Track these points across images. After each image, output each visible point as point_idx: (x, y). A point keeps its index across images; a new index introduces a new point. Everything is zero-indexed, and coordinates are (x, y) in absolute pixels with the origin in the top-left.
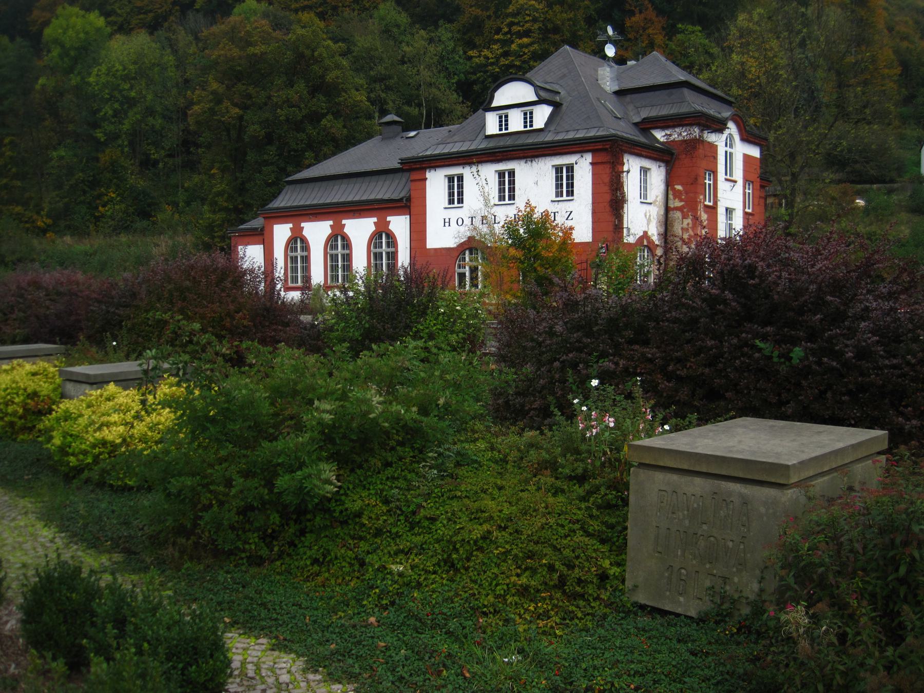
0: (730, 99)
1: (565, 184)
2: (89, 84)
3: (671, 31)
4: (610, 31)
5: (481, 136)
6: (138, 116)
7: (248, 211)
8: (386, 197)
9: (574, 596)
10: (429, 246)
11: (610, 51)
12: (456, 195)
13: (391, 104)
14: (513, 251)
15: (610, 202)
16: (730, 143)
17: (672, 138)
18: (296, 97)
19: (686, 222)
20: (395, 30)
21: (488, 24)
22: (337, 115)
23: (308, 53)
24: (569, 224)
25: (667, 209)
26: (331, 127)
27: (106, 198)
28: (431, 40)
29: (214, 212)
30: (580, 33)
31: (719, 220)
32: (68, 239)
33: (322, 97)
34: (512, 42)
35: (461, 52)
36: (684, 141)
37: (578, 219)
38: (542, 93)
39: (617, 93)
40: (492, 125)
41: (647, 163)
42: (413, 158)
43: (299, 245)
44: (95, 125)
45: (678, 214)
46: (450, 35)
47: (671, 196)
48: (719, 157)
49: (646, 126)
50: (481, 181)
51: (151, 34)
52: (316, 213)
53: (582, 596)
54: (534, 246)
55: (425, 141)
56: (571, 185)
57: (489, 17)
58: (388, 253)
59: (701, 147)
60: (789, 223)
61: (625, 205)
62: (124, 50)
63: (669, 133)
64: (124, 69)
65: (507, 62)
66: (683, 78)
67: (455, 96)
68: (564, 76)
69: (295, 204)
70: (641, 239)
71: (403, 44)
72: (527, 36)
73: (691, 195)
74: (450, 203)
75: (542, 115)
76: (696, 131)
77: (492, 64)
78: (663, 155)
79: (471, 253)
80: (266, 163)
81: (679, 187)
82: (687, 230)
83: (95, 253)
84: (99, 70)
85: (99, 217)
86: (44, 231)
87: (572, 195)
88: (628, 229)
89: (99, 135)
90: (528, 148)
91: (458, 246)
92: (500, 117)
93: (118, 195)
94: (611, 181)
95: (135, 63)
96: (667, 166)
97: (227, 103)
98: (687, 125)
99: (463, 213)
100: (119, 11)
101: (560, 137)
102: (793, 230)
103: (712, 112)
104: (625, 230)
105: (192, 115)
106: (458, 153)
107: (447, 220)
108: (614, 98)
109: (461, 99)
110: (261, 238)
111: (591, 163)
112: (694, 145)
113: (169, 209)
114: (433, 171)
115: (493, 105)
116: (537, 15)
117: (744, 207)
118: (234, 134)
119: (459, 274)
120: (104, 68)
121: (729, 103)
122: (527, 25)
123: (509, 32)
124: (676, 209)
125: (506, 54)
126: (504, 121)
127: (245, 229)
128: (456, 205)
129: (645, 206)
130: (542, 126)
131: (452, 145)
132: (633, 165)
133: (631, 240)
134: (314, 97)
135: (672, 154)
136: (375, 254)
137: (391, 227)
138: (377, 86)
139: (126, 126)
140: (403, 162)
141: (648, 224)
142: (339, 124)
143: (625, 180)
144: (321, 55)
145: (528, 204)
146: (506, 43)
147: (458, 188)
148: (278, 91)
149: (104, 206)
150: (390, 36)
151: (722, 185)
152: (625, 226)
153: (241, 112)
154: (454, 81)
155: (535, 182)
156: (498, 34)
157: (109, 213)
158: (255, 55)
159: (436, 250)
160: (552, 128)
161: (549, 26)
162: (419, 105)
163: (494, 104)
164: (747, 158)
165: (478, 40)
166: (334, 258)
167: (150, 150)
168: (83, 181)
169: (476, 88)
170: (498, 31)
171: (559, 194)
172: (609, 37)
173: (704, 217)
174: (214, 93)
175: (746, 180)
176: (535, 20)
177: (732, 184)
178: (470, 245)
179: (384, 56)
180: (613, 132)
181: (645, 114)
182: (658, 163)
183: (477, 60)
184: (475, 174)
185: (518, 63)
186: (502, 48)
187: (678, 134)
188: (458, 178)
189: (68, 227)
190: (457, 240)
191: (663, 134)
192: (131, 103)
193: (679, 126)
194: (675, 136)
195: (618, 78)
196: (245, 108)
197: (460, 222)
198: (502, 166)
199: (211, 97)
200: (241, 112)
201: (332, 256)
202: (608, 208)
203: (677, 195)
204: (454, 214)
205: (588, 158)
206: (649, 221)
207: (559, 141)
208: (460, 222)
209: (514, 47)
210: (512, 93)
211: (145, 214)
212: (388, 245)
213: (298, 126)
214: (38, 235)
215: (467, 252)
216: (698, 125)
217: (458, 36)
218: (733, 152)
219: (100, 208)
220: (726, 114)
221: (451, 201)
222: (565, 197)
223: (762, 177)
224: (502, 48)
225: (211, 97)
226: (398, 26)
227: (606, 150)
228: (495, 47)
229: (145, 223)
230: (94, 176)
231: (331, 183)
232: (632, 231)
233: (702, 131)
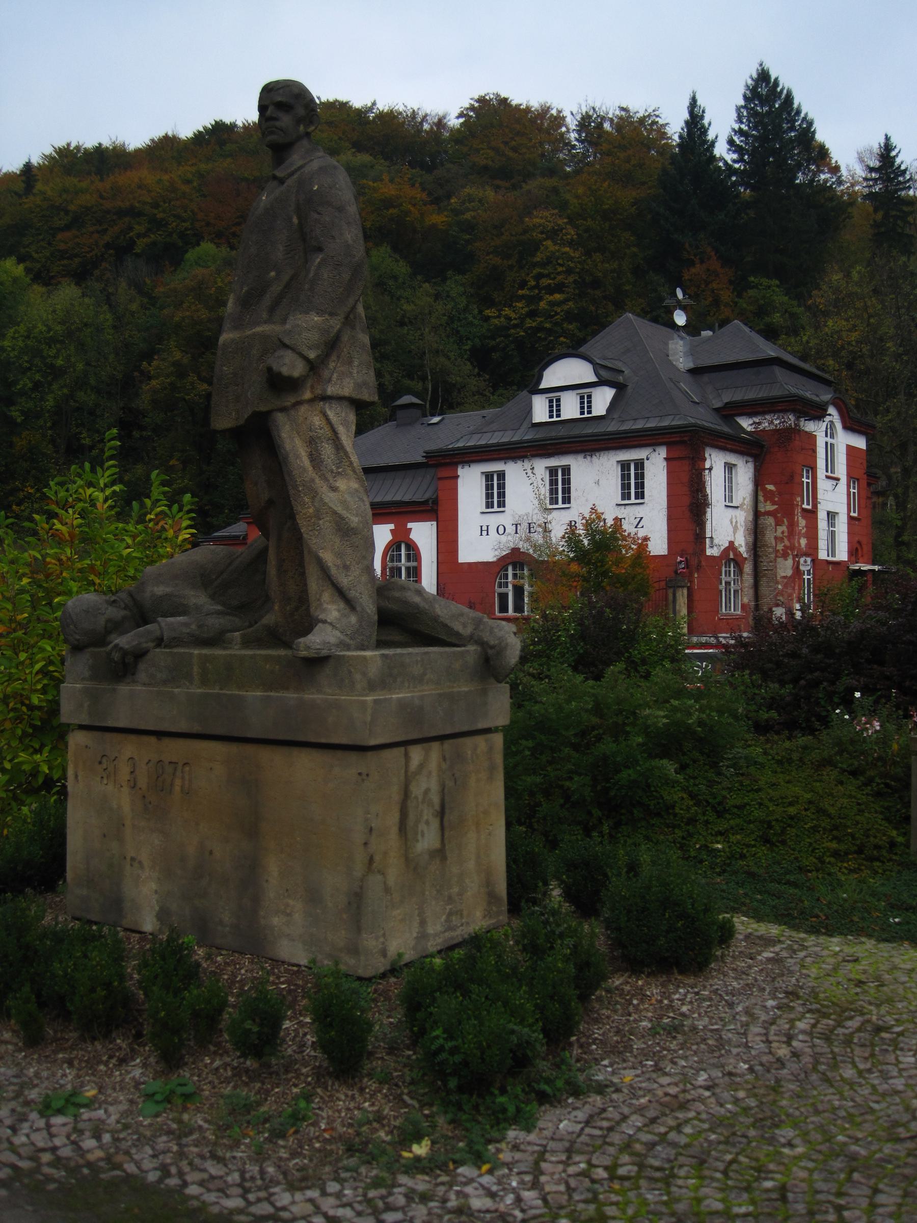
0: (826, 376)
1: (633, 485)
3: (740, 286)
4: (680, 294)
5: (526, 425)
6: (65, 391)
8: (407, 498)
9: (872, 859)
10: (461, 559)
11: (680, 319)
12: (496, 494)
14: (574, 567)
15: (689, 506)
16: (830, 432)
17: (761, 427)
19: (780, 529)
20: (391, 282)
24: (641, 533)
28: (437, 297)
34: (541, 299)
35: (476, 311)
36: (776, 431)
37: (650, 524)
38: (603, 373)
39: (692, 371)
40: (540, 411)
41: (732, 458)
42: (440, 451)
45: (770, 520)
46: (462, 289)
47: (761, 498)
48: (818, 449)
49: (729, 412)
50: (525, 483)
51: (78, 284)
53: (877, 859)
54: (602, 561)
56: (640, 486)
57: (511, 267)
58: (408, 569)
60: (900, 531)
61: (709, 510)
64: (50, 330)
65: (534, 324)
66: (773, 354)
67: (469, 366)
70: (727, 550)
71: (403, 301)
72: (561, 291)
74: (487, 507)
75: (602, 400)
76: (791, 419)
77: (515, 326)
78: (751, 448)
79: (514, 569)
81: (771, 487)
82: (782, 539)
84: (16, 332)
87: (643, 498)
89: (15, 413)
90: (585, 439)
91: (499, 560)
92: (551, 401)
95: (62, 323)
96: (755, 462)
97: (193, 377)
99: (506, 519)
100: (35, 255)
102: (905, 538)
103: (808, 395)
106: (498, 445)
107: (485, 528)
108: (688, 377)
109: (476, 370)
114: (466, 467)
115: (542, 386)
116: (572, 265)
119: (500, 595)
120: (22, 328)
121: (827, 383)
122: (559, 278)
124: (768, 513)
125: (532, 314)
126: (555, 406)
127: (222, 537)
128: (496, 509)
129: (730, 510)
130: (604, 413)
131: (489, 435)
132: (716, 462)
135: (762, 446)
136: (392, 569)
139: (50, 403)
140: (429, 455)
141: (735, 533)
143: (707, 478)
145: (593, 510)
146: (532, 300)
147: (499, 488)
150: (385, 290)
151: (823, 485)
152: (708, 535)
154: (467, 347)
155: (596, 484)
156: (522, 289)
160: (616, 416)
161: (588, 279)
162: (424, 379)
163: (543, 385)
164: (850, 450)
167: (81, 433)
169: (495, 356)
170: (523, 285)
171: (626, 495)
172: (678, 301)
173: (802, 523)
174: (176, 364)
175: (850, 477)
176: (569, 271)
177: (834, 482)
178: (514, 559)
180: (693, 421)
181: (727, 397)
182: (746, 458)
183: (496, 321)
184: (529, 472)
185: (548, 325)
186: (527, 306)
187: (769, 423)
188: (499, 476)
190: (497, 553)
191: (751, 422)
192: (56, 373)
193: (769, 412)
194: (766, 424)
195: (692, 352)
197: (501, 530)
198: (554, 462)
203: (769, 496)
204: (493, 521)
205: (662, 452)
206: (735, 529)
207: (625, 432)
208: (501, 530)
209: (543, 304)
210: (566, 371)
212: (408, 558)
215: (510, 568)
216: (794, 411)
218: (835, 443)
220: (826, 397)
221: (489, 505)
222: (633, 500)
223: (868, 473)
224: (527, 306)
226: (395, 278)
227: (682, 442)
228: (519, 305)
232: (716, 541)
233: (798, 418)
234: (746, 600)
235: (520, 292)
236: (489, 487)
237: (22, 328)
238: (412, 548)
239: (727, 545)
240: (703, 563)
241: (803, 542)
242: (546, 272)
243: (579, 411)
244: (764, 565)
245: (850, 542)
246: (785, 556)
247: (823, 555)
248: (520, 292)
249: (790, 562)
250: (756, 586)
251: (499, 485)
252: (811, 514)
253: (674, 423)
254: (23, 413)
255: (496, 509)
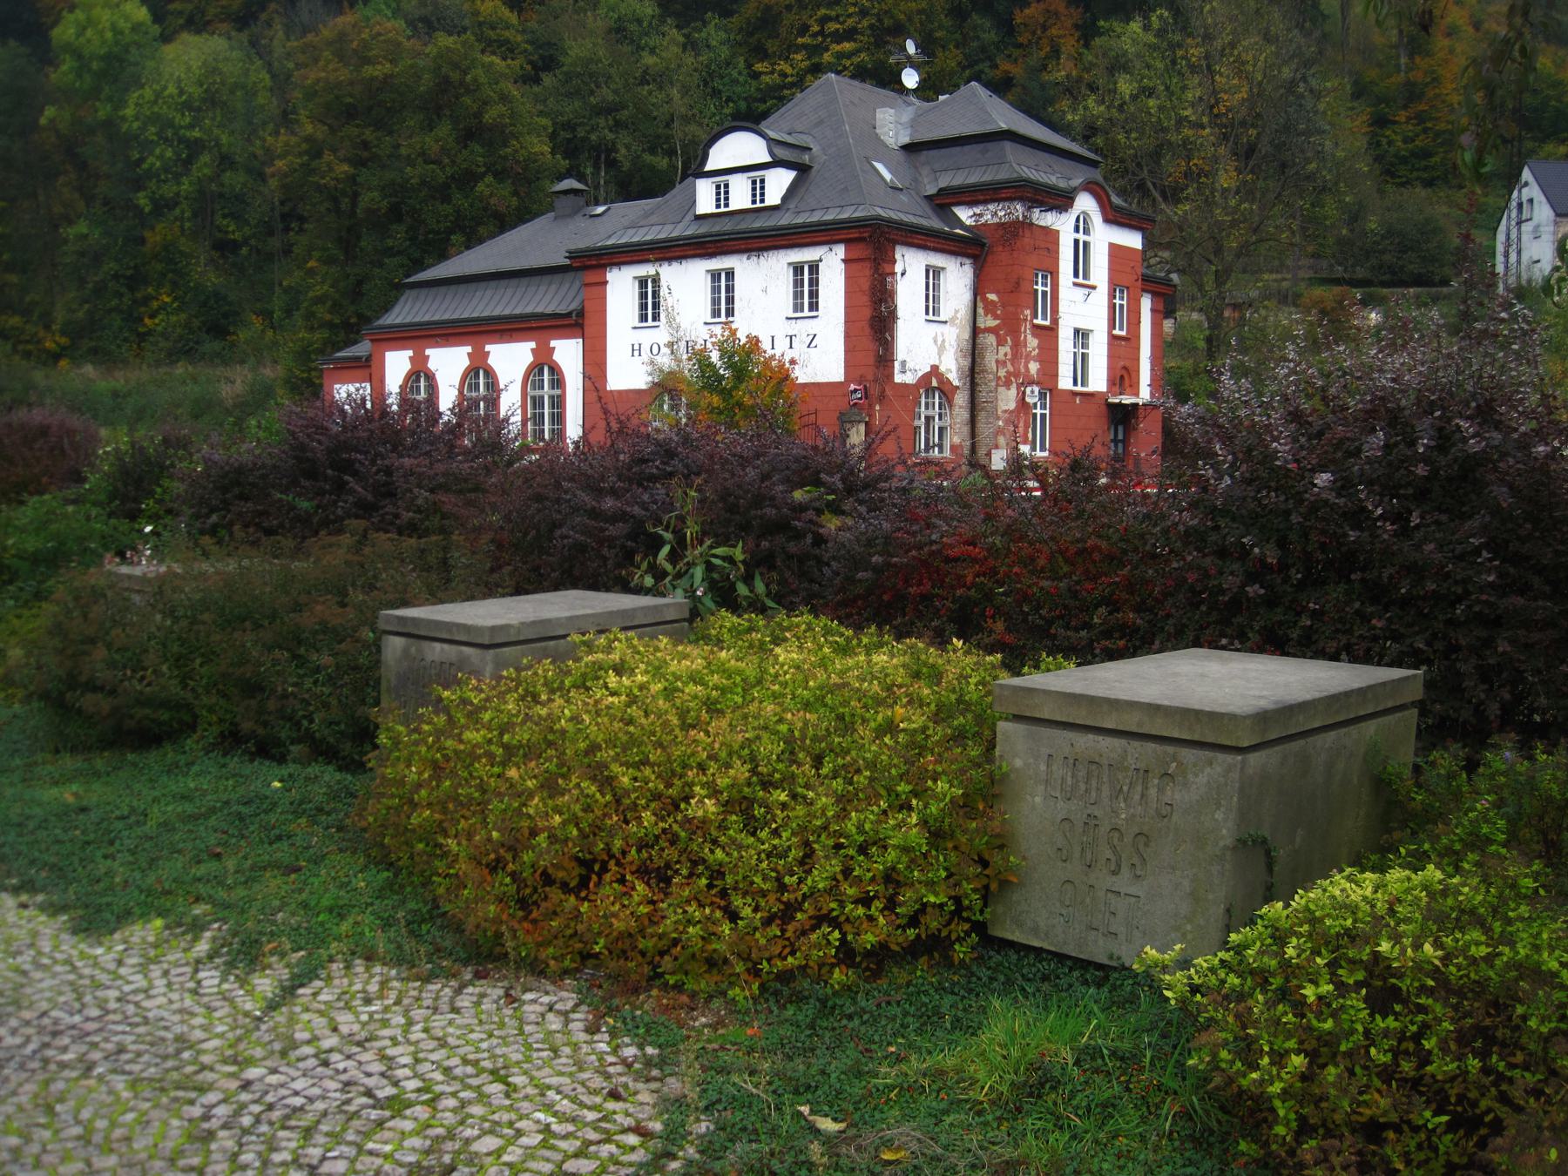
2: (124, 119)
4: (911, 47)
7: (354, 326)
8: (549, 311)
11: (910, 79)
12: (650, 305)
13: (623, 151)
15: (873, 321)
18: (436, 148)
19: (1003, 350)
21: (789, 19)
22: (500, 175)
23: (455, 76)
25: (975, 331)
26: (491, 195)
27: (155, 304)
29: (312, 329)
30: (938, 34)
31: (1061, 348)
32: (89, 369)
33: (478, 148)
35: (742, 65)
36: (1000, 225)
39: (910, 148)
41: (937, 260)
42: (582, 251)
43: (422, 384)
44: (138, 185)
46: (723, 35)
47: (980, 311)
49: (943, 202)
50: (687, 283)
52: (448, 333)
55: (617, 222)
58: (552, 397)
59: (1027, 233)
62: (189, 58)
63: (978, 211)
64: (181, 92)
68: (821, 122)
69: (417, 320)
70: (926, 378)
73: (1011, 309)
74: (795, 310)
75: (778, 183)
76: (1019, 209)
78: (971, 247)
79: (672, 399)
80: (390, 253)
81: (992, 297)
83: (129, 394)
85: (145, 334)
86: (56, 357)
88: (904, 363)
89: (142, 200)
93: (175, 299)
94: (873, 288)
98: (1005, 200)
101: (799, 220)
104: (897, 365)
105: (273, 175)
110: (366, 372)
111: (844, 261)
112: (1013, 231)
113: (257, 323)
114: (675, 265)
115: (707, 168)
117: (1112, 325)
118: (345, 203)
120: (148, 93)
122: (850, 22)
123: (821, 32)
124: (988, 330)
126: (722, 193)
127: (343, 358)
128: (650, 323)
130: (778, 202)
132: (911, 267)
133: (909, 379)
134: (466, 147)
135: (983, 245)
136: (533, 398)
137: (556, 357)
138: (602, 122)
140: (572, 255)
142: (505, 190)
144: (475, 80)
147: (811, 285)
148: (410, 137)
149: (152, 317)
153: (352, 170)
157: (159, 328)
158: (373, 79)
159: (620, 392)
160: (792, 206)
162: (671, 153)
165: (772, 46)
166: (538, 402)
168: (116, 277)
170: (804, 29)
172: (909, 57)
173: (1033, 343)
174: (308, 139)
177: (1086, 291)
179: (613, 71)
181: (945, 181)
182: (959, 260)
186: (809, 58)
187: (992, 214)
188: (811, 268)
189: (94, 351)
192: (195, 147)
194: (988, 217)
196: (359, 163)
199: (304, 146)
200: (352, 170)
201: (533, 398)
202: (868, 330)
203: (990, 308)
205: (840, 251)
206: (941, 350)
209: (827, 57)
211: (219, 330)
213: (442, 193)
214: (45, 364)
216: (1021, 199)
217: (739, 38)
219: (147, 321)
224: (809, 58)
225: (304, 146)
226: (639, 21)
228: (799, 57)
229: (217, 345)
230: (136, 267)
231: (473, 286)
234: (957, 440)
235: (800, 40)
236: (798, 283)
237: (148, 93)
238: (555, 370)
239: (928, 369)
240: (888, 392)
241: (1034, 367)
242: (833, 14)
243: (750, 198)
244: (983, 396)
245: (1110, 368)
246: (1008, 384)
247: (1065, 382)
248: (800, 40)
249: (1013, 391)
250: (973, 421)
251: (811, 280)
252: (1049, 334)
253: (856, 215)
254: (152, 200)
255: (806, 313)
